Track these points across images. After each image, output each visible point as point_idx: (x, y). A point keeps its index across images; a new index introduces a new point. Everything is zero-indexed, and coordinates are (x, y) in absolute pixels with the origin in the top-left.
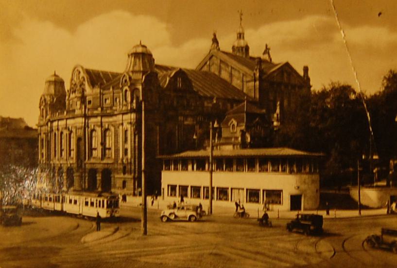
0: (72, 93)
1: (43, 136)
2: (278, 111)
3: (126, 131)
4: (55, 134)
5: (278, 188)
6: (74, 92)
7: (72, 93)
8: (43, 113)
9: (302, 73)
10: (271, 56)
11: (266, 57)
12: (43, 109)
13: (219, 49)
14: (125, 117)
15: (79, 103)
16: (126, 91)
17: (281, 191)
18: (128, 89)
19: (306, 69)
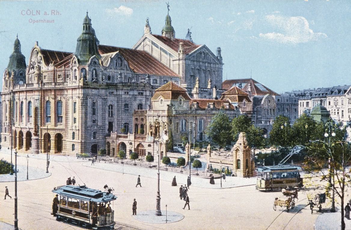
0: (31, 69)
1: (8, 103)
2: (197, 86)
3: (75, 103)
4: (17, 102)
5: (173, 187)
6: (33, 68)
7: (31, 69)
8: (7, 83)
9: (216, 54)
10: (18, 218)
11: (188, 39)
12: (7, 81)
13: (151, 33)
14: (75, 92)
15: (36, 79)
16: (75, 70)
17: (172, 186)
18: (77, 69)
19: (219, 51)
